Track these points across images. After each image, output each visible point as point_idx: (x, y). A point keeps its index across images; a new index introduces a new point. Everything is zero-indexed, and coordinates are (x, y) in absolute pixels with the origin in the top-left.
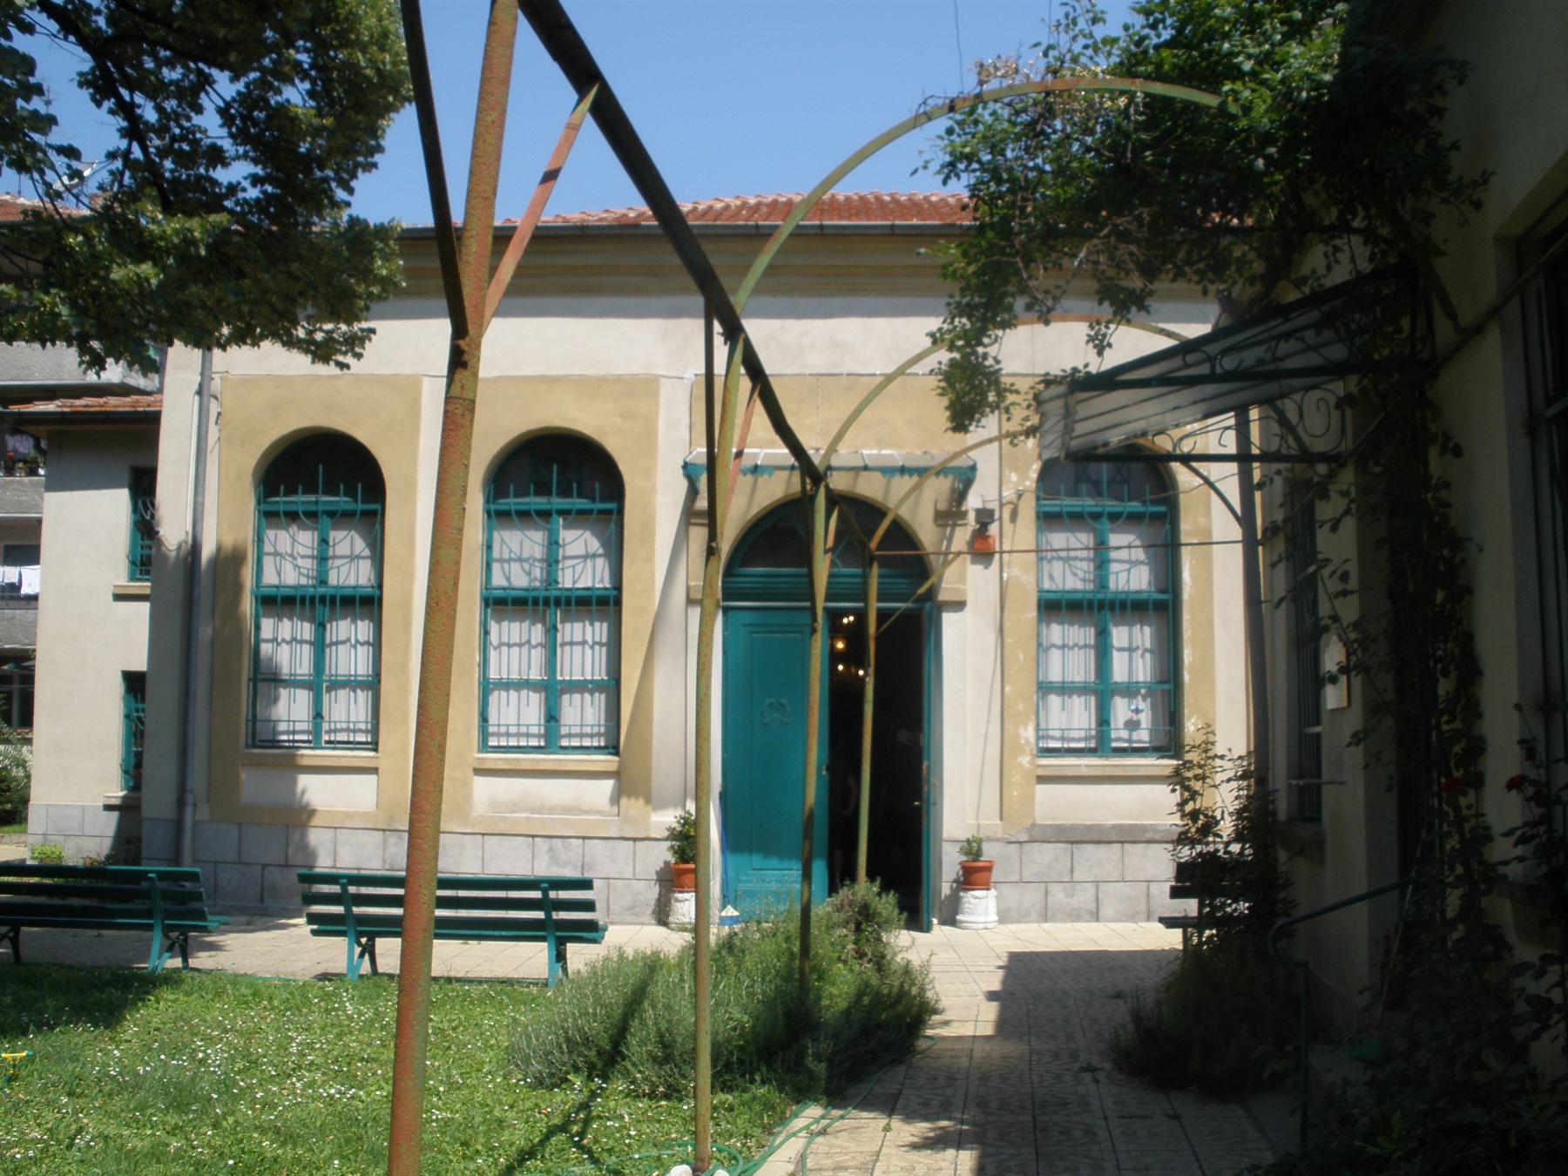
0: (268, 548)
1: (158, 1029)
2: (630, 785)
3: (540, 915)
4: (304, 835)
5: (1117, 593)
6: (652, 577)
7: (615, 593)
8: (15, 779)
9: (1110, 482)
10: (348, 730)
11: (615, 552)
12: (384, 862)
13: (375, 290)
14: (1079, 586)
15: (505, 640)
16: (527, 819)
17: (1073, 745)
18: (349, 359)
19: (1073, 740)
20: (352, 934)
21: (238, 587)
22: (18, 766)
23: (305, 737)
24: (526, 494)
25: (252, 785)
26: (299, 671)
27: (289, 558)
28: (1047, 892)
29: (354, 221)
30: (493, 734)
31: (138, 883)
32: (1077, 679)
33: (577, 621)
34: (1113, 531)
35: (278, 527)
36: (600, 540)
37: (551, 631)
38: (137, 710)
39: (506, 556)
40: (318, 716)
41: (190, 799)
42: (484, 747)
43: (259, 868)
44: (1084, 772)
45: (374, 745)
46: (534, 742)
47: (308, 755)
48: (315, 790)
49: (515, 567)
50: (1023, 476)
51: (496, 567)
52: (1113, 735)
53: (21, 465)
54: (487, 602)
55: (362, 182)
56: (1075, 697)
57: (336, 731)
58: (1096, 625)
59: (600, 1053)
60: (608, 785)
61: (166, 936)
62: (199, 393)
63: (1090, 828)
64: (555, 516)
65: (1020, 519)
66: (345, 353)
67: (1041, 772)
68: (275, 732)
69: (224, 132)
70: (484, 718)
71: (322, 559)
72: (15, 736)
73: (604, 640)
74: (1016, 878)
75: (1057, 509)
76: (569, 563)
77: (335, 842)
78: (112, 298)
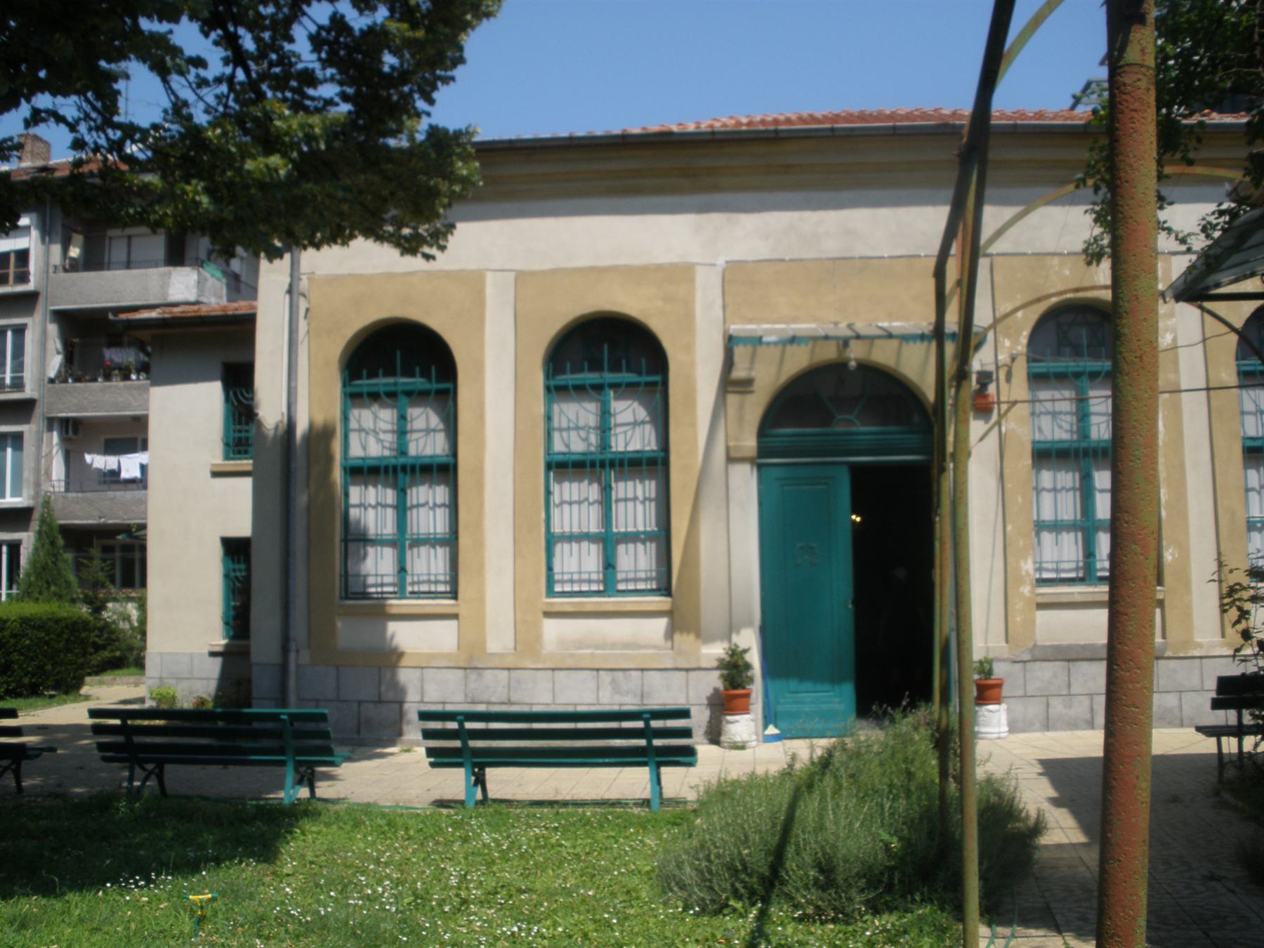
0: (353, 424)
1: (311, 863)
2: (681, 621)
3: (642, 742)
4: (394, 675)
5: (1099, 441)
6: (695, 439)
7: (662, 454)
8: (123, 631)
9: (1089, 346)
10: (429, 582)
11: (662, 420)
12: (466, 696)
13: (457, 188)
14: (1066, 436)
15: (567, 498)
16: (592, 654)
17: (1064, 575)
18: (433, 251)
19: (1064, 571)
20: (469, 766)
21: (329, 459)
22: (124, 620)
23: (390, 589)
24: (581, 370)
25: (347, 633)
26: (385, 532)
27: (371, 433)
28: (1048, 705)
29: (434, 132)
30: (559, 581)
31: (250, 724)
32: (1066, 518)
33: (630, 479)
34: (1092, 388)
35: (362, 406)
36: (647, 408)
37: (606, 490)
38: (234, 570)
39: (564, 425)
40: (402, 570)
41: (293, 646)
42: (550, 592)
43: (355, 705)
44: (1078, 598)
45: (454, 594)
46: (594, 587)
47: (396, 605)
48: (403, 635)
49: (573, 434)
50: (1015, 342)
51: (556, 435)
52: (1098, 565)
53: (117, 372)
54: (549, 466)
55: (442, 94)
56: (1064, 534)
57: (419, 583)
58: (1080, 470)
59: (762, 878)
60: (662, 623)
61: (297, 771)
62: (290, 291)
63: (1084, 647)
64: (607, 389)
65: (1014, 380)
66: (431, 246)
67: (1040, 600)
68: (365, 586)
69: (314, 57)
70: (550, 568)
71: (402, 432)
72: (121, 595)
73: (653, 495)
74: (1021, 693)
75: (1044, 370)
76: (619, 430)
77: (422, 680)
78: (246, 187)
